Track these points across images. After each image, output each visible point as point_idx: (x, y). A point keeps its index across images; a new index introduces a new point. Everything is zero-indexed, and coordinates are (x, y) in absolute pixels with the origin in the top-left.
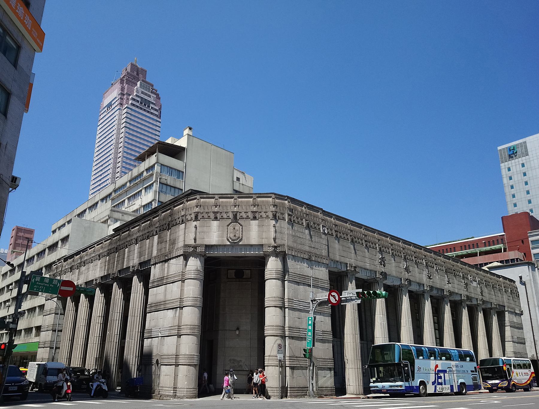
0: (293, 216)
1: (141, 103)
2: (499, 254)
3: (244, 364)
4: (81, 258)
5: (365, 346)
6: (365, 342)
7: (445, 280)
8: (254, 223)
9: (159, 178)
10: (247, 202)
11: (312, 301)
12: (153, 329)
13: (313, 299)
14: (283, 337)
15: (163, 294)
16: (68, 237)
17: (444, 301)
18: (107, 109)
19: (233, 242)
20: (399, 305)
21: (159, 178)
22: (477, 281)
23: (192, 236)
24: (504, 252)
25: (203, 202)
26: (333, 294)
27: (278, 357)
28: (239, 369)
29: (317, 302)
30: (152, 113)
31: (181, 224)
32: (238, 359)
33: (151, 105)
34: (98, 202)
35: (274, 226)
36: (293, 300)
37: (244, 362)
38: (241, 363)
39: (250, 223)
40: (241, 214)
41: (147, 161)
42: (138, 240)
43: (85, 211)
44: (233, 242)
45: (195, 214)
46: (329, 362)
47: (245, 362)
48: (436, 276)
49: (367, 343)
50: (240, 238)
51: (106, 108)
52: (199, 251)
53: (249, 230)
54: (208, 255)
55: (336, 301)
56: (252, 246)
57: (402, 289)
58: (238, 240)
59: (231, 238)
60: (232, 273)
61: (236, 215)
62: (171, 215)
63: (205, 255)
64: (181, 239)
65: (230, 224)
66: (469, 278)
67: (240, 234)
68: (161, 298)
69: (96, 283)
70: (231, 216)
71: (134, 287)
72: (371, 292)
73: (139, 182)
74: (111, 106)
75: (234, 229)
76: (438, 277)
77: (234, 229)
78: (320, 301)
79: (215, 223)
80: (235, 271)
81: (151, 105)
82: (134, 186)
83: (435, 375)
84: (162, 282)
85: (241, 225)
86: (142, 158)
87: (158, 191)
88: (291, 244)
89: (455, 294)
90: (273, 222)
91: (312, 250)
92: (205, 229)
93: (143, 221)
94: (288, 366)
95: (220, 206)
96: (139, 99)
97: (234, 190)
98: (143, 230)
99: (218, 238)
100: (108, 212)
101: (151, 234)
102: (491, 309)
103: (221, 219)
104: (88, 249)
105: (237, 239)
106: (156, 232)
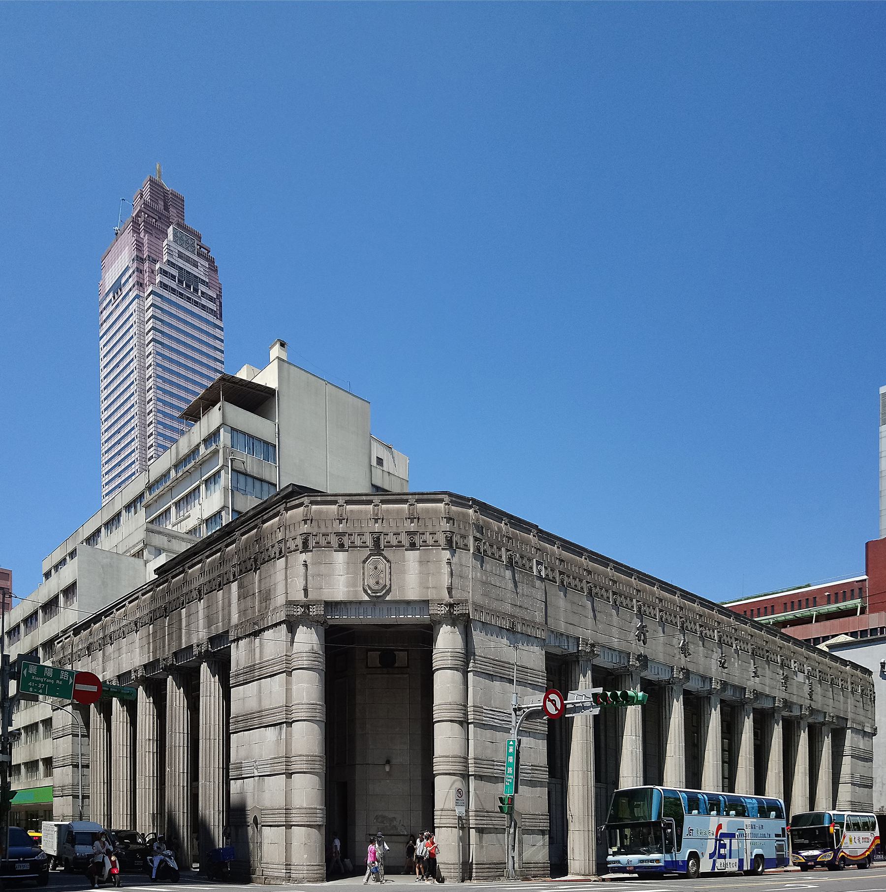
0: (484, 541)
1: (181, 282)
2: (851, 618)
3: (401, 825)
4: (103, 628)
5: (603, 791)
6: (604, 786)
7: (750, 670)
8: (412, 556)
9: (231, 459)
10: (399, 512)
11: (515, 710)
12: (243, 762)
13: (516, 707)
14: (465, 776)
15: (255, 698)
16: (74, 584)
17: (744, 710)
18: (114, 297)
19: (374, 595)
20: (666, 718)
21: (231, 459)
22: (806, 672)
23: (300, 583)
24: (860, 614)
25: (315, 511)
26: (553, 696)
27: (457, 812)
28: (392, 832)
29: (524, 712)
30: (204, 307)
31: (278, 559)
32: (391, 815)
33: (202, 288)
34: (120, 512)
35: (449, 563)
36: (482, 708)
37: (400, 821)
38: (395, 822)
39: (404, 556)
40: (388, 538)
41: (204, 420)
42: (202, 591)
43: (98, 531)
44: (375, 597)
45: (303, 538)
46: (541, 821)
47: (402, 821)
48: (734, 663)
49: (607, 786)
50: (387, 588)
51: (111, 295)
52: (315, 613)
53: (403, 572)
54: (331, 622)
55: (556, 710)
56: (408, 603)
57: (672, 688)
58: (384, 591)
59: (370, 588)
60: (374, 658)
61: (378, 538)
62: (258, 539)
63: (325, 622)
64: (280, 589)
65: (367, 559)
66: (793, 667)
67: (388, 580)
68: (252, 705)
69: (137, 677)
70: (369, 542)
71: (203, 685)
72: (619, 693)
73: (192, 469)
74: (121, 290)
75: (376, 568)
76: (738, 664)
77: (376, 568)
78: (529, 710)
79: (340, 557)
80: (380, 653)
81: (202, 288)
82: (183, 476)
83: (716, 842)
84: (252, 675)
85: (388, 561)
86: (193, 415)
87: (230, 488)
88: (479, 599)
89: (764, 697)
90: (447, 554)
91: (518, 612)
92: (323, 569)
93: (208, 553)
94: (473, 828)
95: (347, 519)
96: (175, 272)
97: (372, 485)
98: (209, 570)
99: (347, 587)
100: (141, 535)
101: (225, 579)
102: (823, 724)
103: (351, 547)
104: (114, 610)
105: (382, 589)
106: (234, 575)
